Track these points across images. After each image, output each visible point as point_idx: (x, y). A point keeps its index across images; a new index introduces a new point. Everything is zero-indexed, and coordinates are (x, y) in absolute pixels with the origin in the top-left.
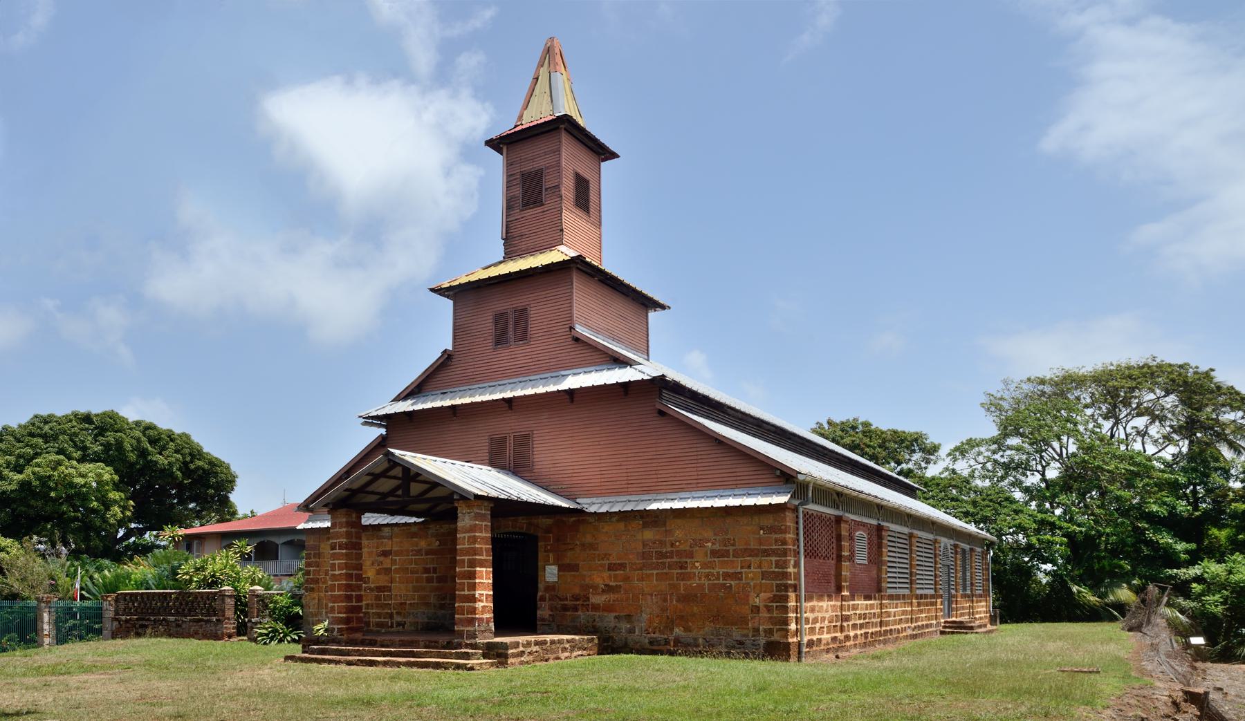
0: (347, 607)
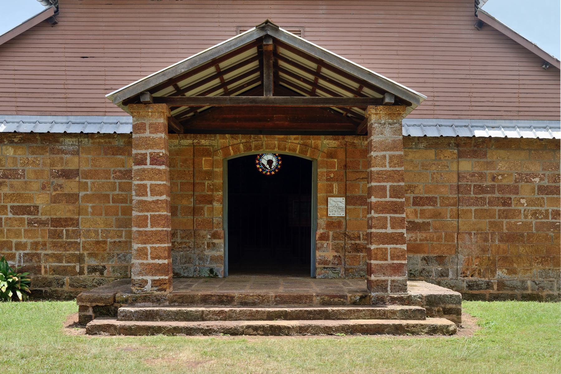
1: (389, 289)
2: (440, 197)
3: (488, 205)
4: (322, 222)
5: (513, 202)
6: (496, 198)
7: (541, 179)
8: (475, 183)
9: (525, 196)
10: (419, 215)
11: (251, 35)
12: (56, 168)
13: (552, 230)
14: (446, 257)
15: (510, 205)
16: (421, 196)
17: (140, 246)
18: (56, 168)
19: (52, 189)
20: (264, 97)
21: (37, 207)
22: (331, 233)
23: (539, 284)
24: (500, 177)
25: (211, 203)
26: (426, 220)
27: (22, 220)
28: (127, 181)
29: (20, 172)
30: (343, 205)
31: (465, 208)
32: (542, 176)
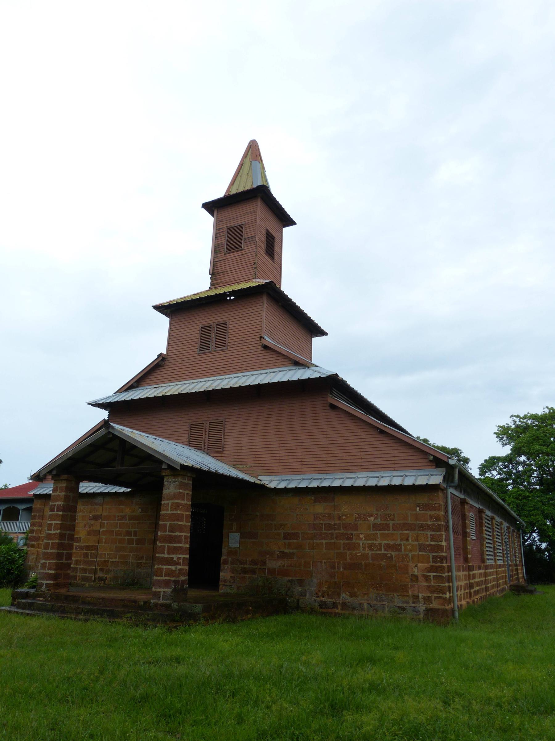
0: (56, 564)
2: (302, 533)
3: (335, 539)
4: (225, 551)
5: (354, 537)
6: (341, 533)
7: (375, 518)
8: (326, 522)
9: (363, 532)
10: (287, 546)
11: (102, 433)
12: (92, 514)
13: (385, 560)
14: (304, 580)
15: (352, 539)
16: (289, 532)
18: (92, 514)
22: (230, 559)
23: (373, 606)
24: (344, 517)
26: (292, 551)
28: (124, 522)
30: (238, 539)
31: (318, 541)
32: (376, 516)
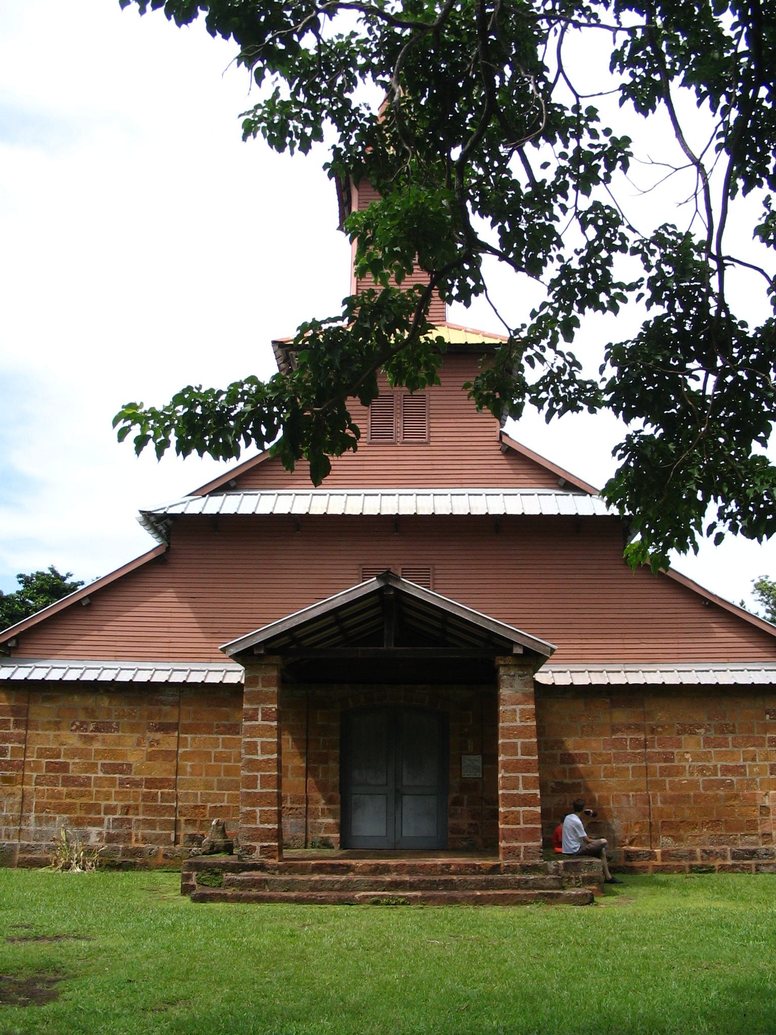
1: (522, 856)
5: (676, 757)
15: (672, 761)
17: (249, 808)
19: (147, 745)
20: (385, 648)
21: (130, 766)
22: (466, 797)
25: (327, 763)
27: (112, 782)
29: (114, 725)
